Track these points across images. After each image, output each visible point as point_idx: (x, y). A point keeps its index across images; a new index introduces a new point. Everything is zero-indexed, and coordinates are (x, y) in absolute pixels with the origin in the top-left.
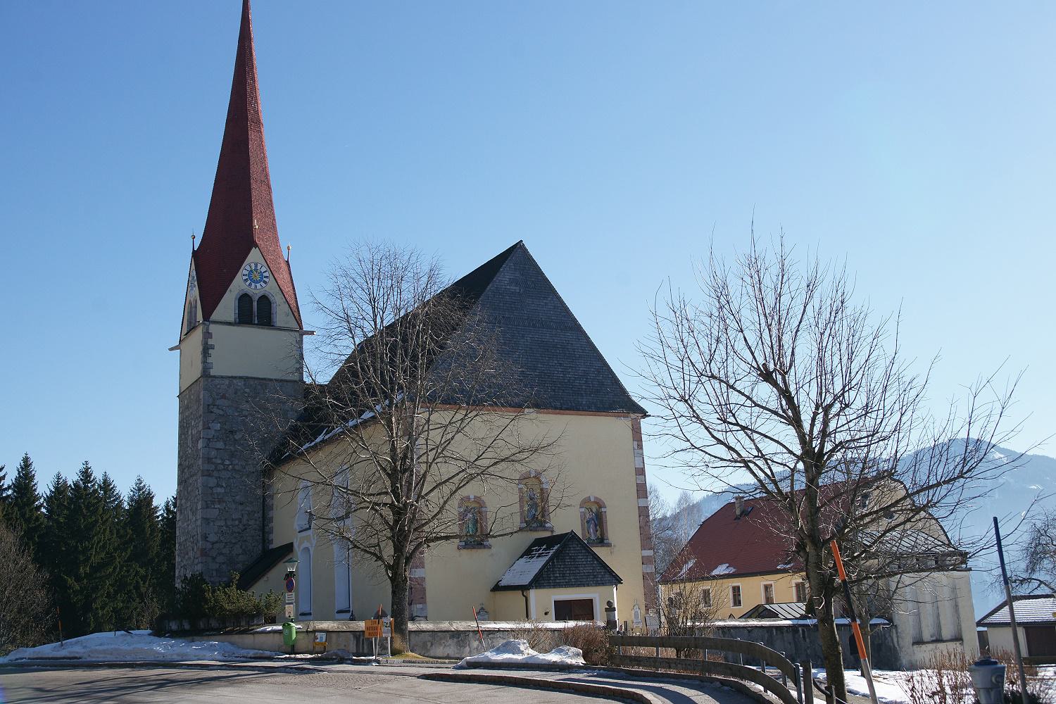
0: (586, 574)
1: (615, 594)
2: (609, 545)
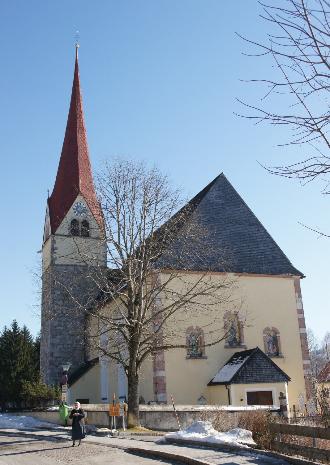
0: (267, 375)
1: (286, 388)
2: (282, 357)
